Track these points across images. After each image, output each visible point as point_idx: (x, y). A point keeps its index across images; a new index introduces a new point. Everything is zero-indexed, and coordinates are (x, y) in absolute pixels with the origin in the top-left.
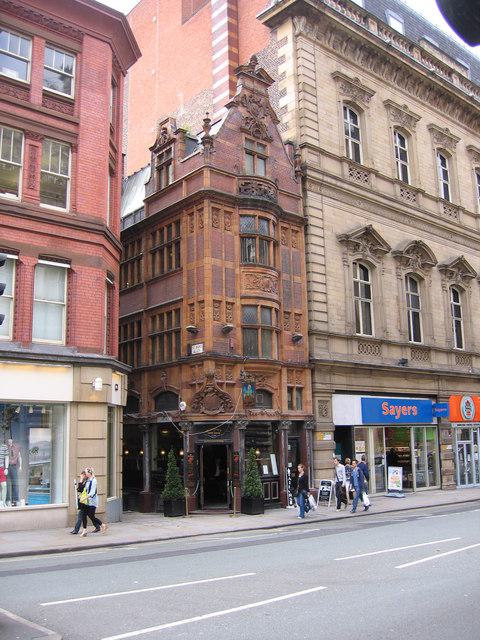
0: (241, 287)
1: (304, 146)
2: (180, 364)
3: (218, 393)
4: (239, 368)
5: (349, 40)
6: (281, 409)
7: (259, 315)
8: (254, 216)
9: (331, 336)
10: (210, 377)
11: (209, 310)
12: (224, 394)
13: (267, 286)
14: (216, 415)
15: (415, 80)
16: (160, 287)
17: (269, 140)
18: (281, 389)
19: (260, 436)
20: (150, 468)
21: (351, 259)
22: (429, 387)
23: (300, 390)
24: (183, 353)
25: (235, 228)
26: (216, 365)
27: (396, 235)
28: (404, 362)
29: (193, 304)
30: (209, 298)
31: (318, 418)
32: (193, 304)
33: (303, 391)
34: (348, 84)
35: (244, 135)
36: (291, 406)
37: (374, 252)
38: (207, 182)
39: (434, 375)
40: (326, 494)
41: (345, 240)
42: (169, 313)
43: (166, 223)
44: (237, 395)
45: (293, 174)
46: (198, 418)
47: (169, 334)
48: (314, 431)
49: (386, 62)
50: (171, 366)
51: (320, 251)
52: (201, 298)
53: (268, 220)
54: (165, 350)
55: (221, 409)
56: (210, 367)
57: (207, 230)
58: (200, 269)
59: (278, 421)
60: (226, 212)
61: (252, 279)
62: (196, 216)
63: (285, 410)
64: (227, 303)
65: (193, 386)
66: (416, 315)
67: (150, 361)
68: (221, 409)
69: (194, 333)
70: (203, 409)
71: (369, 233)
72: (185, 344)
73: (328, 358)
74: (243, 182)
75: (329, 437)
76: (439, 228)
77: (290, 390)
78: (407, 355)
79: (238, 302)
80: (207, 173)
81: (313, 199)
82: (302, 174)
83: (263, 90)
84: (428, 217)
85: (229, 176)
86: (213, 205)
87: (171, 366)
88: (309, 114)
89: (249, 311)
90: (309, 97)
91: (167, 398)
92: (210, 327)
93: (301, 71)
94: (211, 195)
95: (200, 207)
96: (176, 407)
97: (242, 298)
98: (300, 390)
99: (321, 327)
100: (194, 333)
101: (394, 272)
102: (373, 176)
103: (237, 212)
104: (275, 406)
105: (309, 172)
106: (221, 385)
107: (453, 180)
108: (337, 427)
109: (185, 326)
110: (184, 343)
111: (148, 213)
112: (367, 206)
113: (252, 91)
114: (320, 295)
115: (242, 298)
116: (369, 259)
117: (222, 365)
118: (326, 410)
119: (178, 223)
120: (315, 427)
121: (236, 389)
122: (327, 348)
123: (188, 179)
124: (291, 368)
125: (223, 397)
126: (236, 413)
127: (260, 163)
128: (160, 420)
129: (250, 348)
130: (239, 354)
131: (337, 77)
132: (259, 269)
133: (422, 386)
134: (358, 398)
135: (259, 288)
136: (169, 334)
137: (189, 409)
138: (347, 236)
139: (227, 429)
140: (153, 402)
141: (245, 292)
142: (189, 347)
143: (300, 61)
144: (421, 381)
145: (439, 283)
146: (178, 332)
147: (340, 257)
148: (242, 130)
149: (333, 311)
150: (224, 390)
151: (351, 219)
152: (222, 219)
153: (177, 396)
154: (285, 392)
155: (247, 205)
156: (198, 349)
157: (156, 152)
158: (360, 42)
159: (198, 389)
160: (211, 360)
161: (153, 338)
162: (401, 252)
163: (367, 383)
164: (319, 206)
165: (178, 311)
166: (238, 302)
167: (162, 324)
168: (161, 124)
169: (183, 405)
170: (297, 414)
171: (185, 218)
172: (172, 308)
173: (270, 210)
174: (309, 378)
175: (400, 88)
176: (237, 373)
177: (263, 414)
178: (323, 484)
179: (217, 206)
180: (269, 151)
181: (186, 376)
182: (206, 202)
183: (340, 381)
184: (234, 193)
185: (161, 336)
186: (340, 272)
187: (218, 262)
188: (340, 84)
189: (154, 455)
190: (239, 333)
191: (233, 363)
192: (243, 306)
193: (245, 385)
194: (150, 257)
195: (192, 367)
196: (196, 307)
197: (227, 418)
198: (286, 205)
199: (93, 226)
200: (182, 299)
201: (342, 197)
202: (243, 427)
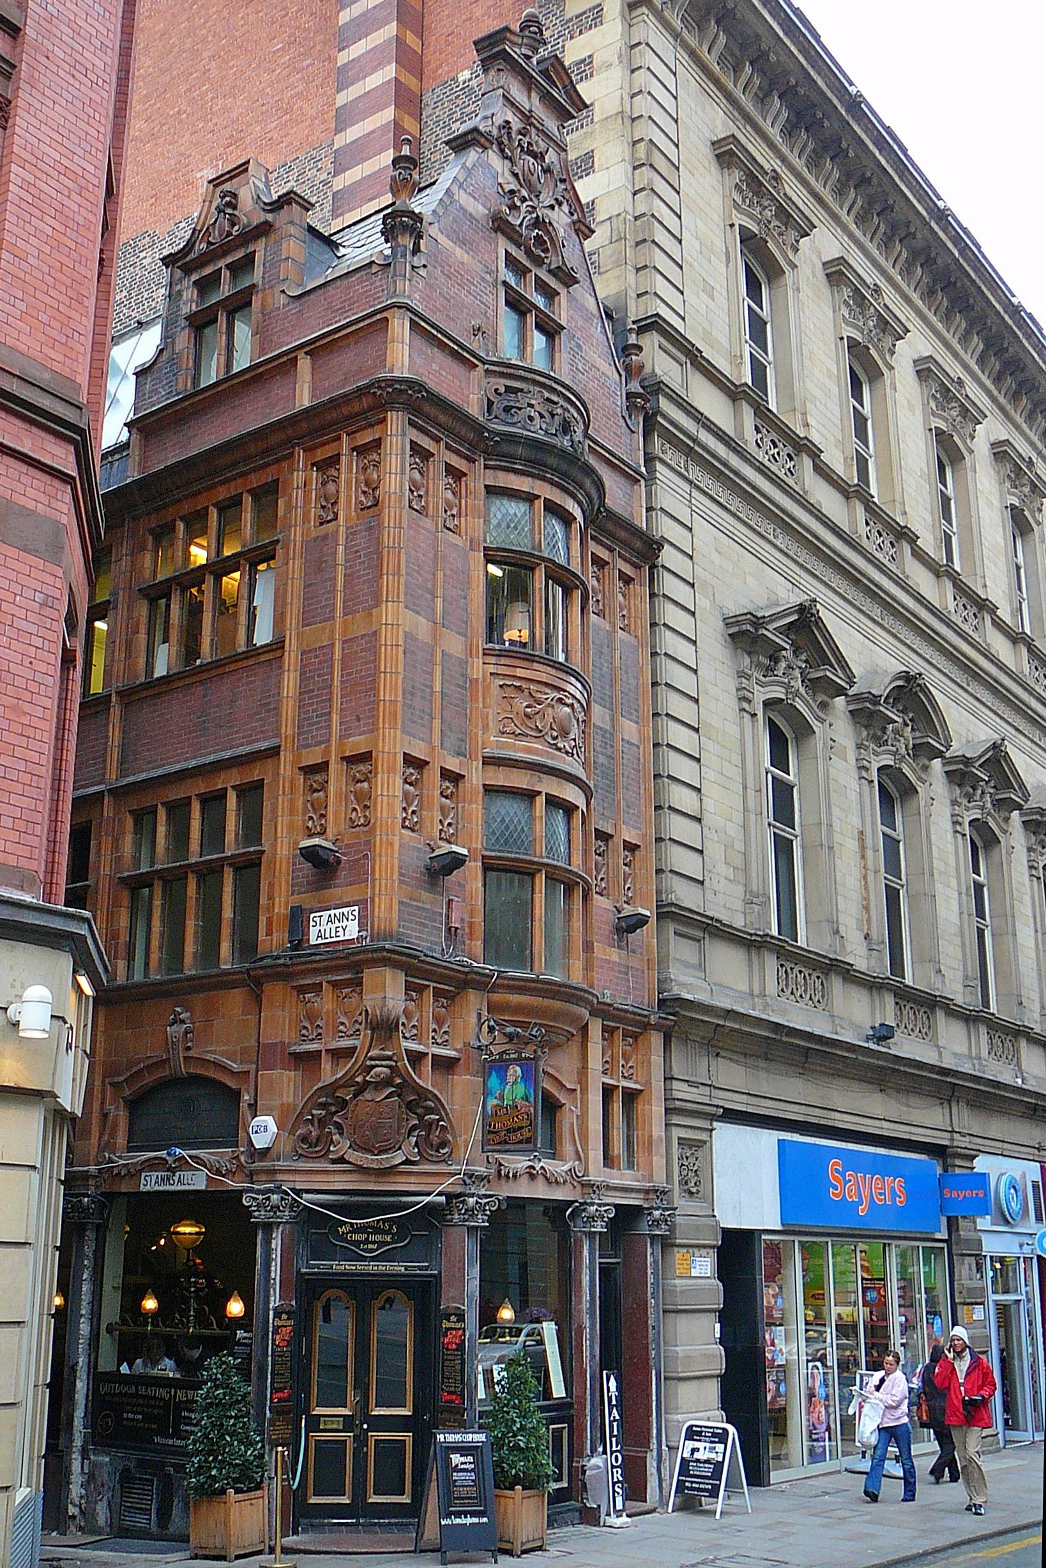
0: (486, 727)
1: (652, 324)
2: (256, 980)
3: (408, 1085)
4: (474, 1003)
5: (759, 61)
6: (582, 1168)
7: (540, 828)
8: (530, 498)
9: (715, 930)
10: (385, 1028)
11: (390, 787)
12: (423, 1094)
13: (564, 733)
14: (391, 1171)
15: (894, 227)
16: (176, 712)
17: (568, 278)
18: (584, 1091)
19: (525, 1247)
20: (93, 1365)
21: (760, 695)
22: (928, 1120)
23: (631, 1097)
24: (272, 941)
25: (473, 525)
26: (409, 987)
27: (870, 654)
28: (883, 1034)
29: (322, 767)
30: (393, 744)
31: (679, 1201)
32: (322, 767)
33: (640, 1106)
34: (755, 185)
35: (503, 245)
36: (608, 1160)
37: (814, 685)
38: (403, 356)
39: (945, 1086)
40: (707, 1471)
41: (746, 635)
42: (213, 801)
43: (222, 493)
44: (464, 1102)
45: (621, 401)
46: (321, 1182)
47: (209, 873)
48: (667, 1244)
49: (839, 155)
50: (215, 983)
51: (684, 651)
52: (357, 743)
53: (567, 519)
54: (191, 925)
55: (409, 1149)
56: (388, 992)
57: (395, 513)
58: (368, 645)
59: (639, 1208)
60: (450, 470)
61: (521, 703)
62: (349, 469)
63: (597, 1172)
64: (446, 774)
65: (307, 1061)
66: (892, 896)
67: (121, 964)
68: (409, 1149)
69: (322, 867)
70: (342, 1146)
71: (805, 624)
72: (281, 908)
73: (702, 997)
74: (501, 383)
75: (704, 1266)
76: (942, 650)
77: (608, 1092)
78: (888, 1012)
79: (476, 776)
80: (400, 326)
81: (670, 490)
82: (645, 401)
83: (551, 125)
84: (924, 614)
85: (462, 357)
86: (414, 435)
87: (224, 982)
88: (661, 237)
89: (510, 808)
90: (661, 187)
91: (197, 1102)
92: (396, 852)
93: (642, 105)
94: (416, 400)
95: (367, 437)
96: (230, 1132)
97: (488, 761)
98: (631, 1097)
99: (685, 896)
100: (322, 867)
101: (851, 755)
102: (808, 463)
103: (480, 477)
104: (568, 1149)
105: (664, 404)
106: (416, 1058)
107: (967, 527)
108: (725, 1231)
109: (283, 841)
110: (279, 895)
111: (143, 464)
112: (793, 548)
113: (527, 117)
114: (686, 791)
115: (488, 761)
116: (800, 705)
117: (421, 989)
118: (697, 1182)
119: (267, 494)
120: (672, 1228)
121: (464, 1082)
122: (702, 967)
123: (317, 349)
124: (626, 1027)
125: (418, 1103)
126: (466, 1170)
127: (538, 340)
128: (150, 1183)
129: (508, 936)
130: (473, 956)
131: (726, 154)
132: (543, 673)
133: (916, 1116)
134: (769, 1139)
135: (539, 735)
136: (209, 873)
137: (285, 1147)
138: (758, 622)
139: (431, 1220)
140: (121, 1116)
141: (496, 743)
142: (298, 920)
143: (641, 76)
144: (914, 1100)
145: (947, 811)
146: (249, 867)
147: (731, 684)
148: (500, 225)
149: (714, 851)
150: (426, 1079)
151: (764, 582)
152: (440, 488)
153: (236, 1095)
154: (595, 1099)
155: (512, 457)
156: (335, 926)
157: (187, 270)
158: (786, 73)
159: (329, 1073)
160: (396, 965)
161: (136, 885)
162: (875, 699)
163: (792, 1092)
164: (684, 514)
165: (252, 792)
166: (476, 776)
167: (180, 837)
168: (216, 182)
169: (264, 1130)
170: (622, 1183)
171: (301, 476)
172: (230, 780)
173: (567, 484)
174: (657, 1059)
175: (858, 233)
176: (471, 1020)
177: (533, 1176)
178: (692, 1434)
179: (426, 443)
180: (563, 314)
181: (280, 1020)
182: (396, 420)
183: (733, 1080)
184: (474, 408)
185: (172, 880)
186: (734, 730)
187: (422, 626)
188: (737, 175)
189: (111, 1311)
190: (472, 876)
191: (454, 985)
192: (488, 790)
193: (500, 1066)
194: (143, 609)
195: (302, 990)
196: (337, 778)
197: (426, 1187)
198: (618, 495)
199: (45, 402)
200: (274, 752)
201: (735, 504)
202: (481, 1221)
